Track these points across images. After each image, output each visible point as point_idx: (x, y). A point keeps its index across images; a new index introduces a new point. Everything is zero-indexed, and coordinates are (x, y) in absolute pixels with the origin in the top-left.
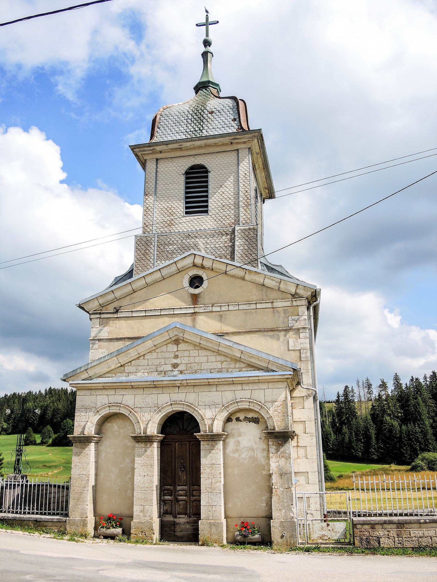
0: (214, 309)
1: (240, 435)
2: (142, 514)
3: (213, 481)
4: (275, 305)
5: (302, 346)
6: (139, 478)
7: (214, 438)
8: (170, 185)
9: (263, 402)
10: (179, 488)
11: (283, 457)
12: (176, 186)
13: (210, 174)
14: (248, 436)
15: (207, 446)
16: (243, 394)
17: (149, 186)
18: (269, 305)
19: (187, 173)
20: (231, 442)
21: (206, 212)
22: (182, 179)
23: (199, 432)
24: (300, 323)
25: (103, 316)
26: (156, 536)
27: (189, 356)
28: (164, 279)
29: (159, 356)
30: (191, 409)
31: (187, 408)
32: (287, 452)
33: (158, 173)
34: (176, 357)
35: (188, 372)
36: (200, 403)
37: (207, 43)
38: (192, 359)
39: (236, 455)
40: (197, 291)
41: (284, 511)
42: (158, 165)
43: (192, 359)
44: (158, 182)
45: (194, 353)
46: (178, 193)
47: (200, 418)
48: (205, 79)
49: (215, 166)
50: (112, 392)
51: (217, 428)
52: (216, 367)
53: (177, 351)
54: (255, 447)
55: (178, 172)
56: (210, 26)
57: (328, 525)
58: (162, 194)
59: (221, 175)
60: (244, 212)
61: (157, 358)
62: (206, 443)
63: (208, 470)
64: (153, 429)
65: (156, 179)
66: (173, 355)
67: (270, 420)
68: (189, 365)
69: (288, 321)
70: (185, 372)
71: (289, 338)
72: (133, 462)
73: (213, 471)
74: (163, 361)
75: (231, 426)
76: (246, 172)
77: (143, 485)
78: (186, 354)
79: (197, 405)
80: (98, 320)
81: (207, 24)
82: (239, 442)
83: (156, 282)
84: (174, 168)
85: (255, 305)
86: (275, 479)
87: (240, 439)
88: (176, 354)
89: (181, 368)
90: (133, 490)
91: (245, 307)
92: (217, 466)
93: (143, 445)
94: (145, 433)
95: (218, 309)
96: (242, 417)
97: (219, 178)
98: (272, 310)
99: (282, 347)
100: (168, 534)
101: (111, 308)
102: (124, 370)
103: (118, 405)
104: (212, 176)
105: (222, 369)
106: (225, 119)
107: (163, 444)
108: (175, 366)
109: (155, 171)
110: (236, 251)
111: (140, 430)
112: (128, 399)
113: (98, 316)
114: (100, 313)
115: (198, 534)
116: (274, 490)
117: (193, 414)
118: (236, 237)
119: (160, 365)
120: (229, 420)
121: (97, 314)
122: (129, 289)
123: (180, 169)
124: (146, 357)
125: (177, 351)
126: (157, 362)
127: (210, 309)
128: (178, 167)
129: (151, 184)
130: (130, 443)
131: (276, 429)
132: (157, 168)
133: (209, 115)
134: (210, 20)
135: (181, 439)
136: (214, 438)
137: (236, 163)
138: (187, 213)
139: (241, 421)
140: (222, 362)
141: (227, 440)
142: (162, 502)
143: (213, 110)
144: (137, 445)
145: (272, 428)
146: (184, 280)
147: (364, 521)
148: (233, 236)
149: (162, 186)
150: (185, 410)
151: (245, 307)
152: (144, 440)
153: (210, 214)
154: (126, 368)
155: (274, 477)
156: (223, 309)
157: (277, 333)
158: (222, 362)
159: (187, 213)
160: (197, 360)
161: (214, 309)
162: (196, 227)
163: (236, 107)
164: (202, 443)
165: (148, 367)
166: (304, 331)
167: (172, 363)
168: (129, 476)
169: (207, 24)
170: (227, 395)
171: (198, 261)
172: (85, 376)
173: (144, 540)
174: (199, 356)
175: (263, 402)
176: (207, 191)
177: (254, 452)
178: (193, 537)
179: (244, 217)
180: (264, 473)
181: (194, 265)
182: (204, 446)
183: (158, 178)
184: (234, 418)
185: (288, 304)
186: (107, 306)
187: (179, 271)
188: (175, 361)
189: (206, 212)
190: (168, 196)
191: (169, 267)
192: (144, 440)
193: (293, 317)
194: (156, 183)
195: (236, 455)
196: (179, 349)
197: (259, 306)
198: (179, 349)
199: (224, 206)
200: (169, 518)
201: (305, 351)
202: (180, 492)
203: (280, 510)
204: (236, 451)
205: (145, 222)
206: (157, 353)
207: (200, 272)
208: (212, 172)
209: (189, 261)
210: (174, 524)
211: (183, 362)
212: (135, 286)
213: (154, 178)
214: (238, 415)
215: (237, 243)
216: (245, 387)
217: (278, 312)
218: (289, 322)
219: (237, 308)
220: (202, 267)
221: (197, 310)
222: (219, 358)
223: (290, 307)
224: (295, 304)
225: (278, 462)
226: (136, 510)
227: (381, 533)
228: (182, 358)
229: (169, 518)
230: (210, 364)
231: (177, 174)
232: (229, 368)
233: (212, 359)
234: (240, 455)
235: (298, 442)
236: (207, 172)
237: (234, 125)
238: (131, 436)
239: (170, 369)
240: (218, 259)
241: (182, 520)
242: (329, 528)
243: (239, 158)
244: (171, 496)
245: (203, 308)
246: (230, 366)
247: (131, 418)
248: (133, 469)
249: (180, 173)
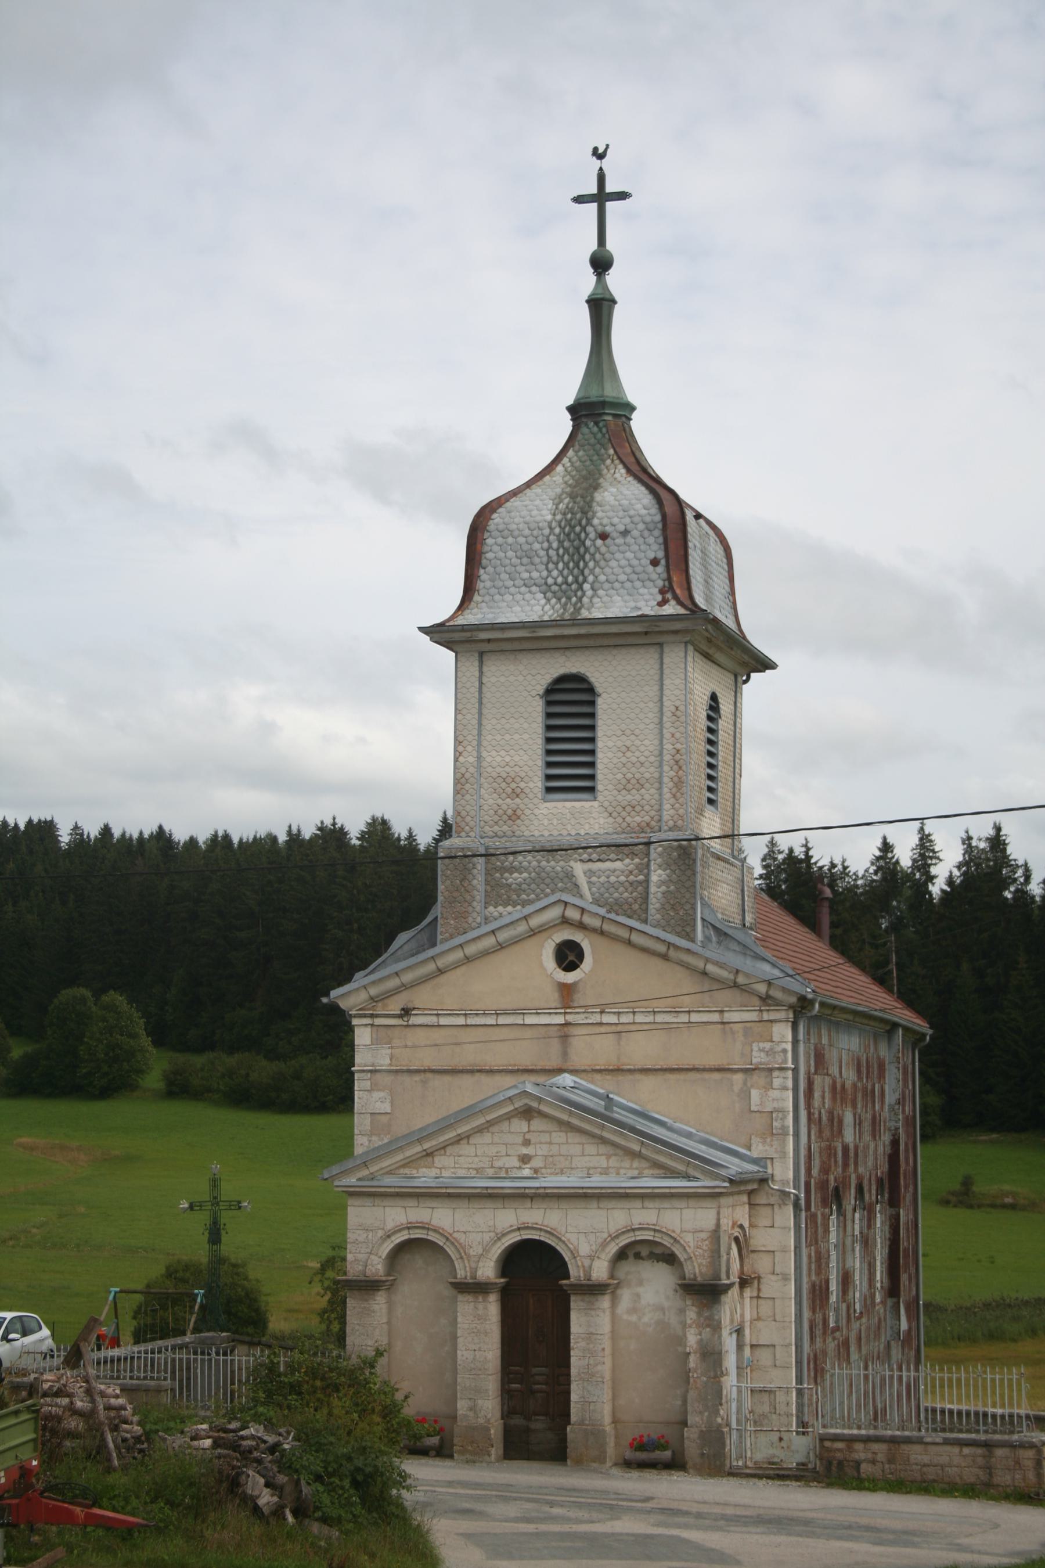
0: (606, 1019)
1: (641, 1283)
2: (471, 1414)
3: (591, 1362)
4: (728, 1017)
5: (775, 1105)
6: (465, 1353)
7: (593, 1290)
8: (512, 721)
9: (678, 1231)
10: (535, 1370)
11: (708, 1326)
12: (526, 725)
13: (600, 701)
14: (652, 1290)
15: (582, 1304)
16: (643, 1216)
17: (465, 722)
18: (715, 1017)
19: (549, 691)
20: (626, 1296)
21: (591, 790)
22: (537, 708)
23: (568, 1277)
24: (774, 1057)
25: (378, 1021)
26: (497, 1450)
27: (550, 1143)
28: (502, 948)
29: (496, 1140)
30: (554, 1239)
31: (547, 1235)
32: (716, 1317)
33: (485, 689)
34: (527, 1143)
35: (549, 1171)
36: (570, 1229)
37: (601, 263)
38: (555, 1149)
39: (634, 1318)
40: (570, 977)
41: (706, 1414)
42: (485, 669)
43: (555, 1149)
44: (485, 711)
45: (559, 1137)
46: (530, 742)
47: (569, 1254)
48: (594, 395)
49: (611, 679)
50: (412, 1202)
51: (600, 1271)
52: (597, 1165)
53: (529, 1132)
54: (666, 1304)
55: (529, 688)
56: (609, 205)
57: (781, 1439)
58: (494, 743)
59: (623, 705)
60: (672, 801)
61: (492, 1143)
62: (579, 1297)
63: (583, 1344)
64: (488, 1270)
65: (480, 703)
66: (520, 1140)
67: (689, 1263)
68: (551, 1159)
69: (752, 1050)
70: (543, 1171)
71: (752, 1086)
72: (454, 1323)
73: (591, 1346)
74: (503, 1150)
75: (626, 1268)
76: (678, 703)
77: (472, 1365)
78: (545, 1138)
79: (563, 1232)
80: (369, 1029)
81: (601, 197)
82: (638, 1295)
83: (486, 953)
84: (521, 678)
85: (687, 1015)
86: (693, 1361)
87: (641, 1290)
88: (527, 1136)
89: (536, 1163)
90: (455, 1372)
91: (668, 1018)
92: (599, 1337)
93: (470, 1298)
94: (474, 1277)
95: (613, 1019)
96: (644, 1252)
97: (619, 711)
98: (720, 1026)
99: (737, 1105)
100: (518, 1446)
101: (395, 1006)
102: (433, 1162)
103: (425, 1227)
104: (605, 706)
105: (607, 1168)
106: (635, 557)
107: (507, 1296)
108: (525, 1159)
109: (477, 684)
110: (651, 896)
111: (462, 1273)
112: (443, 1218)
113: (368, 1021)
114: (372, 1016)
115: (566, 1447)
116: (691, 1380)
117: (558, 1248)
118: (652, 863)
119: (498, 1156)
120: (622, 1255)
121: (365, 1016)
122: (431, 967)
123: (534, 682)
124: (472, 1141)
125: (529, 1132)
126: (493, 1150)
127: (596, 1018)
128: (529, 677)
129: (469, 716)
130: (448, 1292)
131: (699, 1279)
132: (481, 672)
133: (599, 542)
134: (610, 188)
135: (535, 1285)
136: (593, 1290)
137: (657, 677)
138: (549, 790)
139: (642, 1258)
140: (608, 1157)
141: (619, 1292)
142: (506, 1393)
143: (608, 529)
144: (460, 1297)
145: (692, 1276)
146: (544, 952)
147: (835, 1434)
148: (646, 860)
149: (494, 721)
150: (542, 1239)
151: (668, 1018)
152: (475, 1288)
153: (600, 798)
154: (436, 1159)
155: (692, 1358)
156: (624, 1019)
157: (728, 1075)
158: (608, 1157)
159: (549, 790)
160: (564, 1150)
161: (606, 1019)
162: (569, 827)
163: (660, 526)
164: (572, 1298)
165: (476, 1159)
166: (782, 1074)
167: (519, 1153)
168: (446, 1348)
169: (601, 197)
170: (617, 1218)
171: (573, 914)
172: (365, 1173)
173: (476, 1454)
174: (567, 1143)
175: (678, 1231)
176: (592, 740)
177: (664, 1314)
178: (557, 1453)
179: (672, 812)
180: (680, 1349)
181: (565, 921)
182: (576, 1304)
183: (484, 701)
184: (631, 1254)
185: (754, 1016)
186: (386, 1001)
187: (533, 933)
188: (525, 1151)
189: (591, 790)
190: (507, 748)
191: (511, 927)
192: (475, 1288)
193: (762, 1045)
194: (480, 714)
195: (634, 1318)
196: (532, 1128)
197: (695, 1017)
198: (532, 1128)
199: (629, 781)
200: (517, 1421)
201: (780, 1115)
202: (537, 1377)
203: (701, 1412)
204: (633, 1310)
205: (460, 808)
206: (493, 1133)
207: (578, 937)
208: (604, 695)
209: (555, 913)
210: (528, 1430)
211: (540, 1153)
212: (441, 963)
213: (475, 701)
214: (638, 1248)
215: (654, 878)
216: (647, 1204)
217: (733, 1033)
218: (754, 1054)
219: (650, 1019)
220: (581, 926)
221: (570, 1018)
222: (603, 1149)
223: (758, 1024)
224: (766, 1016)
225: (700, 1334)
226: (462, 1406)
227: (862, 1456)
228: (538, 1146)
229: (517, 1421)
230: (587, 1158)
231: (525, 694)
232: (621, 1168)
233: (591, 1149)
234: (640, 1319)
235: (759, 1290)
236: (591, 690)
237: (654, 576)
238: (451, 1283)
239: (517, 1164)
240: (612, 916)
241: (539, 1424)
242: (783, 1444)
243: (665, 666)
244: (521, 1383)
245: (582, 1016)
246: (623, 1165)
247: (448, 1249)
248: (454, 1338)
249: (534, 693)
